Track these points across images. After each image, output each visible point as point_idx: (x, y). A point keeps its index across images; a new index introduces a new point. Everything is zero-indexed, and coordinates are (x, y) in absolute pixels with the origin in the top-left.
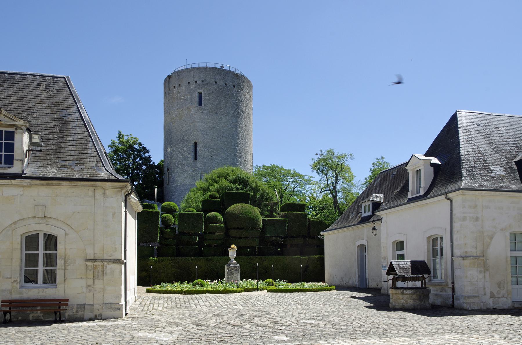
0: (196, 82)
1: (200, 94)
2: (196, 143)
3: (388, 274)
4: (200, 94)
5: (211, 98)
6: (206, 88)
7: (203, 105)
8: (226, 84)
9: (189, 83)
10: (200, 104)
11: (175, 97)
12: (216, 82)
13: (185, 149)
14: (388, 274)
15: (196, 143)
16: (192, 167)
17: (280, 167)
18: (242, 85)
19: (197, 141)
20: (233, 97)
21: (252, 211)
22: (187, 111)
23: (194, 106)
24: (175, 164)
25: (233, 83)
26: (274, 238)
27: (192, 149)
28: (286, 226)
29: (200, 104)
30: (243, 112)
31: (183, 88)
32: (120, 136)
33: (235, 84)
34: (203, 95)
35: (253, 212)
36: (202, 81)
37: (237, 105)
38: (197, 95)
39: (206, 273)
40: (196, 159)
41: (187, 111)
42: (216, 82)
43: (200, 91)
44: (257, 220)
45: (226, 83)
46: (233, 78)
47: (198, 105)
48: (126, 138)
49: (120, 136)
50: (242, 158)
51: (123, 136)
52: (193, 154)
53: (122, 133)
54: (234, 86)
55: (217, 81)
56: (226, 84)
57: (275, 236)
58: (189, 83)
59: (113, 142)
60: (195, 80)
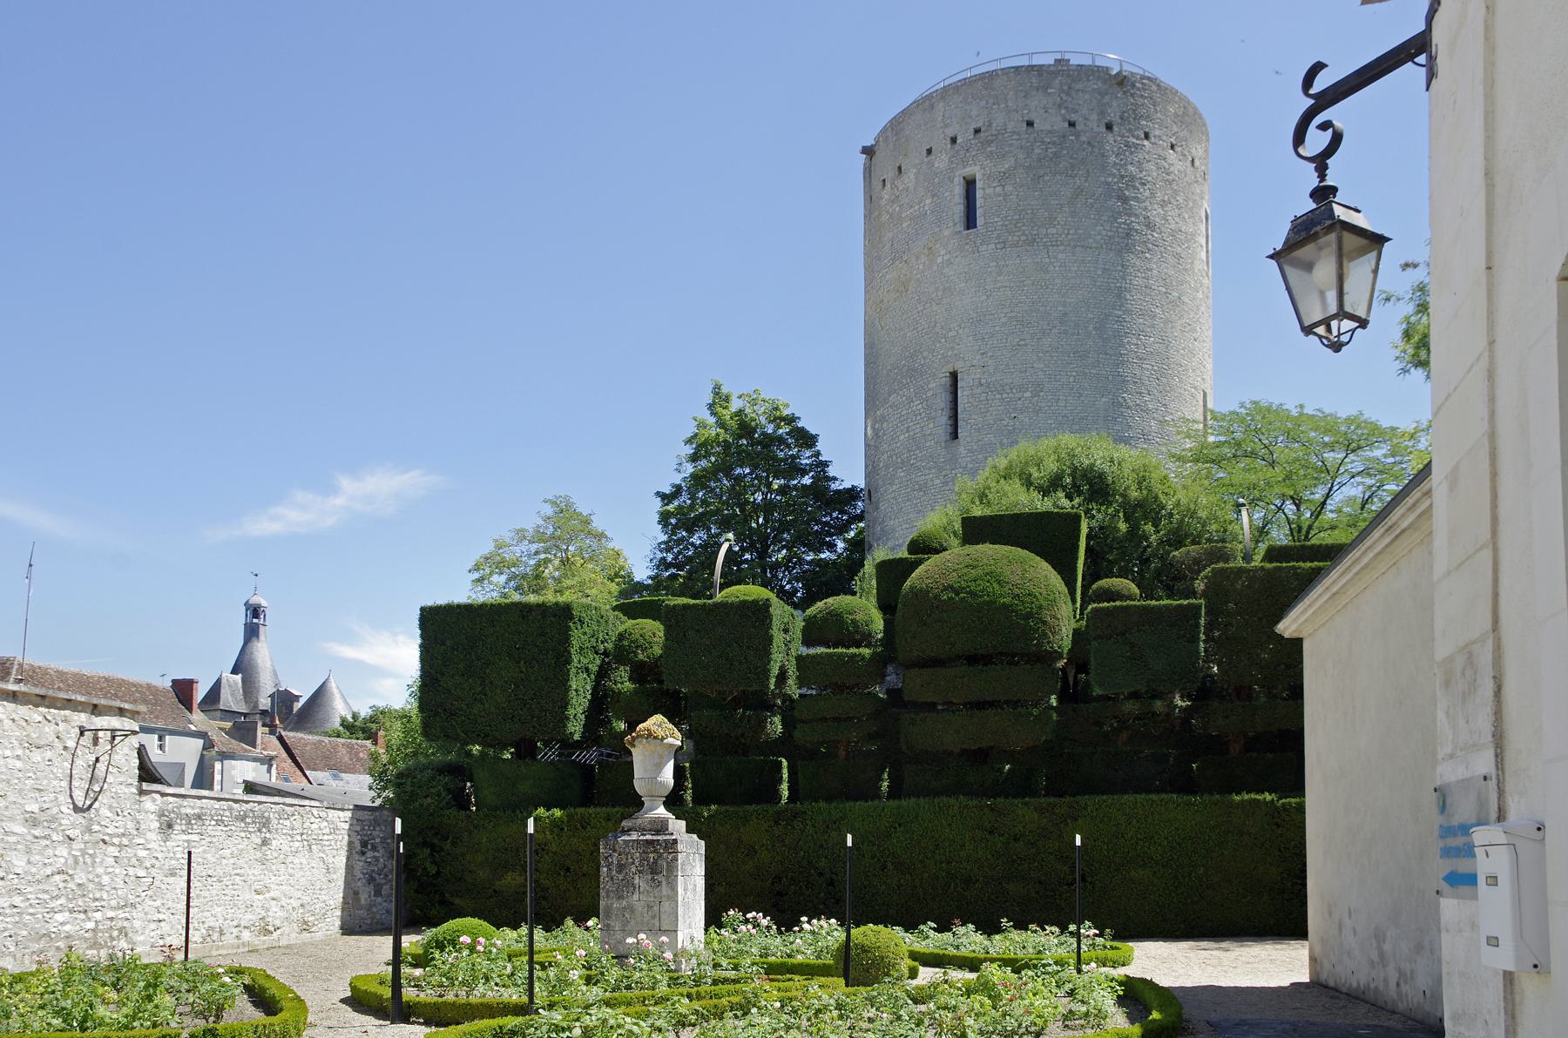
0: (954, 140)
1: (970, 184)
2: (954, 376)
3: (234, 672)
4: (970, 184)
5: (1009, 188)
6: (990, 156)
7: (980, 221)
8: (1072, 124)
9: (929, 151)
10: (970, 221)
11: (885, 217)
12: (1030, 124)
13: (917, 406)
14: (234, 672)
15: (954, 376)
16: (940, 469)
17: (1294, 412)
18: (1148, 118)
19: (959, 366)
20: (1103, 168)
21: (1012, 574)
22: (923, 259)
23: (946, 233)
24: (887, 467)
25: (1102, 113)
26: (1131, 707)
27: (942, 401)
28: (1195, 640)
29: (970, 221)
30: (1150, 225)
31: (910, 177)
32: (719, 399)
33: (1113, 115)
34: (979, 184)
35: (1016, 579)
36: (977, 131)
37: (1125, 200)
38: (958, 190)
39: (778, 879)
40: (955, 435)
41: (923, 259)
42: (1030, 124)
43: (968, 171)
44: (1029, 616)
45: (1073, 117)
46: (1103, 94)
47: (960, 227)
48: (735, 405)
49: (719, 399)
50: (1147, 411)
51: (727, 399)
52: (944, 419)
53: (724, 390)
54: (1109, 127)
55: (1032, 116)
56: (1072, 124)
57: (1135, 695)
58: (929, 151)
59: (702, 425)
60: (950, 132)
